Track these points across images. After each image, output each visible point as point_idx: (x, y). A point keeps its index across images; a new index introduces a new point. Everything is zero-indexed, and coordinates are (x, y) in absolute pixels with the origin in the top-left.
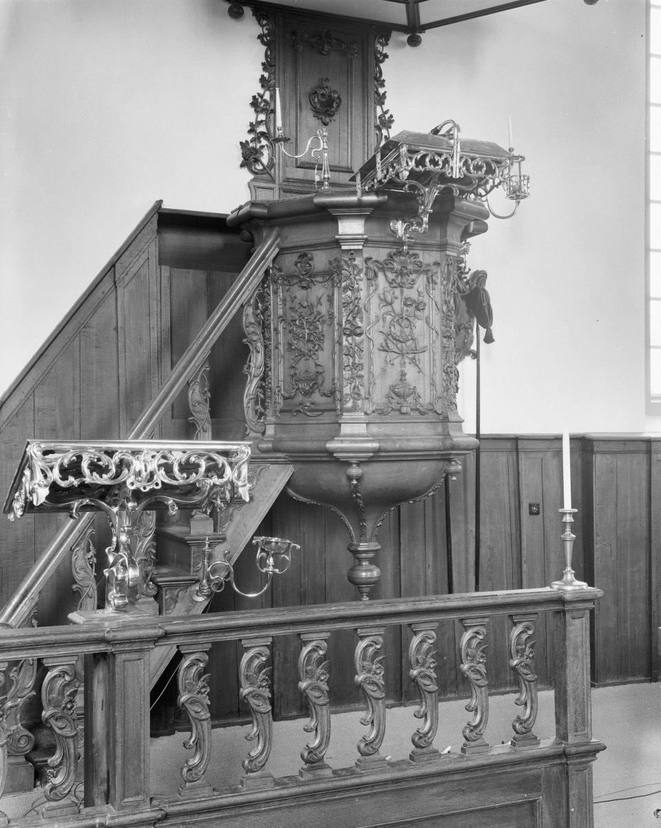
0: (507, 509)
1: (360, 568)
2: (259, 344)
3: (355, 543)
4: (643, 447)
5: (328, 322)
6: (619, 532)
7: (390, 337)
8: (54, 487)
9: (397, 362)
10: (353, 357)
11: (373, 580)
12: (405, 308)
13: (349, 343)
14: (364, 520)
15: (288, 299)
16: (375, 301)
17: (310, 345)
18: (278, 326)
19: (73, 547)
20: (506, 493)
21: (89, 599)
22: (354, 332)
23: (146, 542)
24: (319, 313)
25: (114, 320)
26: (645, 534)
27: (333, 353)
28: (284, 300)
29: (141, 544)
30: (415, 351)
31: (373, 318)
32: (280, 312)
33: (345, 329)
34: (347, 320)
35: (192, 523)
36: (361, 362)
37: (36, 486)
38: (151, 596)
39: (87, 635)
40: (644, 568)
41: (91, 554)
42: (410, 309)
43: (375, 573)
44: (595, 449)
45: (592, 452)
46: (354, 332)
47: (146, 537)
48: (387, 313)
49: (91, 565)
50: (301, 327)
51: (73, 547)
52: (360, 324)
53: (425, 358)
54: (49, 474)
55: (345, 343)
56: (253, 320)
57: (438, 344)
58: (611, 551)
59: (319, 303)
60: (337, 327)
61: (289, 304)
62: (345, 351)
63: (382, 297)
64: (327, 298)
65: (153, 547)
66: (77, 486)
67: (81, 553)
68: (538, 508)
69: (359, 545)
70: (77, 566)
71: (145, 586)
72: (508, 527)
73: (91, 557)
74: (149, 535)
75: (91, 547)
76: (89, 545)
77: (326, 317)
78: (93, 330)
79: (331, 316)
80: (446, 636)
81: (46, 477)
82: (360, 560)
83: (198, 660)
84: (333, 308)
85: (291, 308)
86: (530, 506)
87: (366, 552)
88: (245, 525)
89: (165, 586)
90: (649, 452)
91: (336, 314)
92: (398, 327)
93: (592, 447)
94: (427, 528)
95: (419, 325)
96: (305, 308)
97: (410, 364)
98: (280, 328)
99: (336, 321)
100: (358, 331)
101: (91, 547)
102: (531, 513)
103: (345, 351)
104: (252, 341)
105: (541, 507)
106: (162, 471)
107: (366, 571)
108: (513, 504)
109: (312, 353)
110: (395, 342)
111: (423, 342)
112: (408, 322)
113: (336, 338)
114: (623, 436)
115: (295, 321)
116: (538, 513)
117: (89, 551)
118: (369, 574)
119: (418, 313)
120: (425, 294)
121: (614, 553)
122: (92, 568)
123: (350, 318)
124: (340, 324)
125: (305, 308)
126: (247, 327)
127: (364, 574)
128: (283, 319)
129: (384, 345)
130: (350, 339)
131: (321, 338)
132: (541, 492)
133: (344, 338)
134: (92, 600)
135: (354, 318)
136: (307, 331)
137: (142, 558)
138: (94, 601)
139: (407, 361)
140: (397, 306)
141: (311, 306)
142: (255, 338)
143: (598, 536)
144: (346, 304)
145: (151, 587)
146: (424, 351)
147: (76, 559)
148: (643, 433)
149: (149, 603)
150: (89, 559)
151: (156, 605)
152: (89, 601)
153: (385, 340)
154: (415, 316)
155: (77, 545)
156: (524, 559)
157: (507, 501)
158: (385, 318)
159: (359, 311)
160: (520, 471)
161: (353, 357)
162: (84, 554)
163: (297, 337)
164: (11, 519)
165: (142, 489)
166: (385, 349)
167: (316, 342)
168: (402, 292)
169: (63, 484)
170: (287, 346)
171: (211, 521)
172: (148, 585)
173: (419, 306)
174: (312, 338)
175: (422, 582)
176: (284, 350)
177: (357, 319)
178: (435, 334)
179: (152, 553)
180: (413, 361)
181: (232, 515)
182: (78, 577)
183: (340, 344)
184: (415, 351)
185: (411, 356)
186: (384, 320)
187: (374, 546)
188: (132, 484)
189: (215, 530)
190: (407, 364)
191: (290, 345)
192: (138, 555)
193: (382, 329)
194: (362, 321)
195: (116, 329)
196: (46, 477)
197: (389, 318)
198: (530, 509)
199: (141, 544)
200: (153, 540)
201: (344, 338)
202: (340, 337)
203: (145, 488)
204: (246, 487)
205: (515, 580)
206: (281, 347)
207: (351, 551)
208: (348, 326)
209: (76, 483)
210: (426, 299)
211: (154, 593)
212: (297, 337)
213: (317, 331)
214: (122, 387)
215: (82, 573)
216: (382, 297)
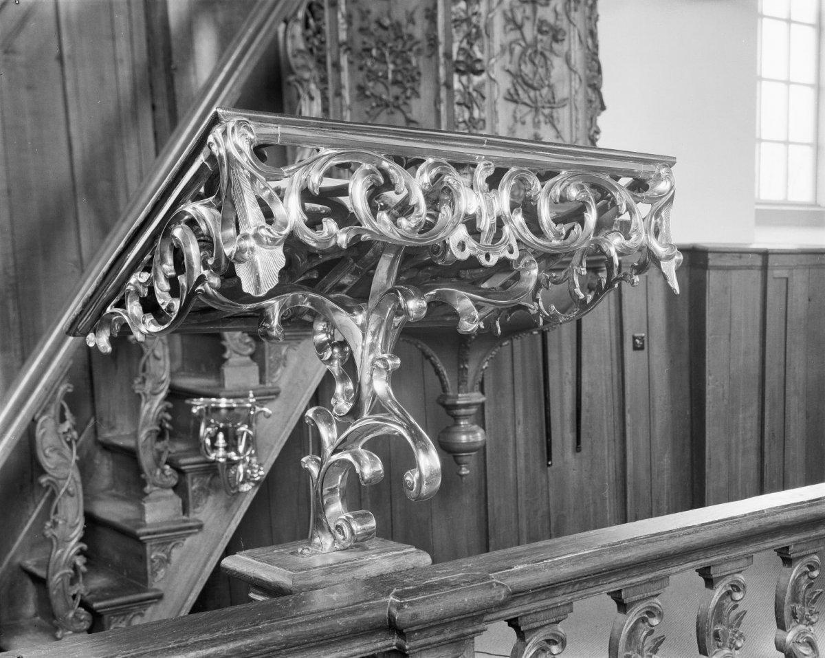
0: (608, 343)
1: (455, 429)
2: (313, 86)
3: (451, 394)
4: (758, 261)
5: (426, 52)
6: (732, 369)
7: (520, 80)
8: (292, 244)
9: (529, 119)
10: (470, 108)
11: (478, 445)
12: (540, 37)
13: (462, 84)
14: (467, 361)
15: (356, 15)
16: (498, 22)
17: (396, 90)
18: (339, 59)
19: (37, 415)
20: (607, 322)
21: (68, 499)
22: (470, 67)
23: (156, 404)
24: (411, 37)
25: (55, 45)
26: (755, 371)
27: (437, 101)
28: (349, 18)
29: (147, 406)
30: (552, 103)
31: (497, 48)
32: (343, 36)
33: (458, 62)
34: (461, 49)
35: (227, 371)
36: (483, 115)
37: (251, 243)
38: (168, 488)
39: (351, 619)
40: (756, 414)
41: (67, 425)
42: (545, 38)
43: (479, 436)
44: (710, 263)
45: (705, 267)
46: (470, 67)
47: (156, 394)
48: (515, 42)
49: (69, 443)
50: (381, 59)
51: (37, 415)
52: (479, 55)
53: (563, 114)
54: (278, 210)
55: (457, 85)
56: (302, 46)
57: (580, 97)
58: (723, 394)
59: (411, 21)
60: (442, 60)
61: (357, 23)
62: (458, 98)
63: (509, 15)
64: (424, 14)
65: (167, 410)
66: (344, 246)
67: (51, 424)
68: (643, 342)
69: (457, 398)
70: (45, 445)
71: (158, 472)
72: (608, 368)
73: (69, 430)
74: (161, 391)
75: (68, 414)
76: (62, 410)
77: (424, 44)
78: (20, 59)
79: (433, 42)
80: (540, 513)
81: (269, 216)
82: (456, 418)
83: (548, 641)
84: (435, 28)
85: (362, 30)
86: (634, 338)
87: (467, 406)
88: (305, 373)
89: (191, 471)
90: (765, 268)
91: (441, 38)
92: (530, 66)
93: (706, 260)
94: (516, 372)
95: (558, 64)
96: (385, 28)
97: (546, 123)
98: (344, 61)
99: (441, 49)
100: (478, 67)
101: (68, 414)
102: (636, 348)
103: (458, 98)
104: (301, 81)
105: (645, 339)
106: (519, 219)
107: (467, 433)
108: (614, 338)
109: (401, 102)
110: (526, 88)
111: (562, 92)
112: (542, 60)
113: (442, 80)
114: (729, 246)
115: (368, 50)
116: (642, 348)
117: (63, 419)
118: (471, 438)
119: (556, 46)
120: (564, 17)
121: (726, 396)
122: (71, 447)
123: (464, 45)
124: (448, 55)
125: (385, 28)
126: (295, 56)
127: (464, 438)
128: (348, 47)
129: (512, 91)
130: (464, 79)
131: (414, 78)
132: (645, 320)
133: (456, 77)
134: (75, 499)
135: (471, 45)
136: (391, 67)
137: (151, 428)
138: (79, 501)
139: (542, 118)
140: (529, 32)
141: (397, 26)
142: (307, 75)
143: (710, 375)
144: (457, 22)
145: (168, 473)
146: (564, 106)
147: (44, 434)
148: (751, 244)
149: (166, 498)
150: (64, 433)
151: (178, 501)
152: (69, 502)
153: (514, 85)
154: (552, 50)
155: (44, 412)
156: (628, 407)
157: (607, 332)
158: (514, 49)
159: (478, 35)
160: (623, 293)
161: (470, 108)
162: (57, 426)
163: (372, 75)
164: (420, 310)
165: (482, 259)
166: (512, 98)
167: (408, 85)
168: (535, 11)
169: (310, 238)
170: (356, 92)
171: (255, 368)
172: (163, 471)
173: (556, 35)
174: (399, 77)
175: (511, 444)
176: (351, 96)
177: (476, 48)
178: (578, 81)
179: (166, 420)
180: (551, 120)
181: (285, 357)
182: (47, 464)
183: (449, 86)
184: (552, 103)
185: (547, 111)
186: (511, 52)
187: (476, 397)
188: (462, 246)
189: (262, 381)
190: (543, 125)
191: (361, 89)
192: (145, 424)
193: (508, 66)
194: (482, 52)
195: (60, 58)
196: (269, 216)
197: (518, 50)
198: (635, 343)
199: (147, 406)
200: (166, 399)
201: (456, 77)
202: (449, 76)
203: (487, 257)
204: (673, 260)
205: (617, 435)
206: (346, 93)
207: (444, 406)
208: (461, 58)
209: (343, 238)
210: (564, 24)
211: (174, 482)
212: (372, 75)
213: (408, 66)
214: (77, 154)
215: (55, 457)
216: (509, 15)
